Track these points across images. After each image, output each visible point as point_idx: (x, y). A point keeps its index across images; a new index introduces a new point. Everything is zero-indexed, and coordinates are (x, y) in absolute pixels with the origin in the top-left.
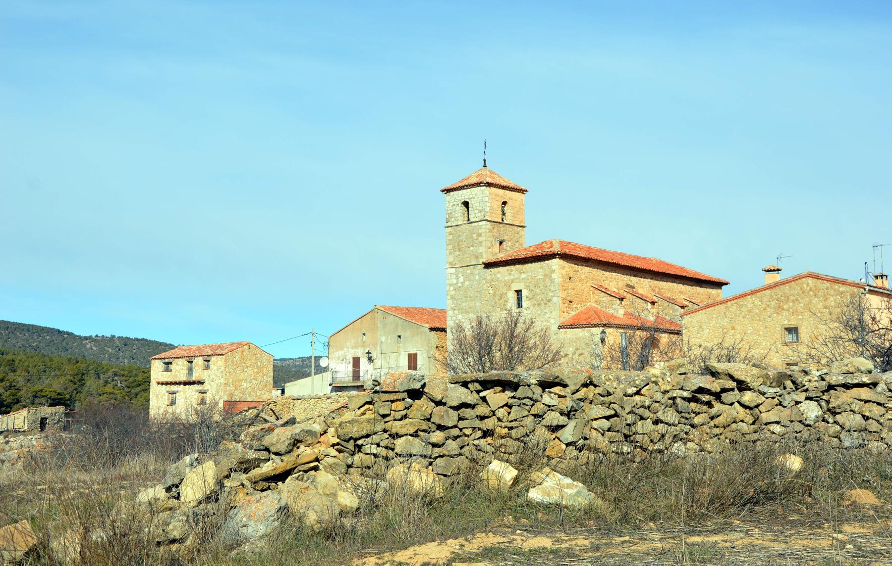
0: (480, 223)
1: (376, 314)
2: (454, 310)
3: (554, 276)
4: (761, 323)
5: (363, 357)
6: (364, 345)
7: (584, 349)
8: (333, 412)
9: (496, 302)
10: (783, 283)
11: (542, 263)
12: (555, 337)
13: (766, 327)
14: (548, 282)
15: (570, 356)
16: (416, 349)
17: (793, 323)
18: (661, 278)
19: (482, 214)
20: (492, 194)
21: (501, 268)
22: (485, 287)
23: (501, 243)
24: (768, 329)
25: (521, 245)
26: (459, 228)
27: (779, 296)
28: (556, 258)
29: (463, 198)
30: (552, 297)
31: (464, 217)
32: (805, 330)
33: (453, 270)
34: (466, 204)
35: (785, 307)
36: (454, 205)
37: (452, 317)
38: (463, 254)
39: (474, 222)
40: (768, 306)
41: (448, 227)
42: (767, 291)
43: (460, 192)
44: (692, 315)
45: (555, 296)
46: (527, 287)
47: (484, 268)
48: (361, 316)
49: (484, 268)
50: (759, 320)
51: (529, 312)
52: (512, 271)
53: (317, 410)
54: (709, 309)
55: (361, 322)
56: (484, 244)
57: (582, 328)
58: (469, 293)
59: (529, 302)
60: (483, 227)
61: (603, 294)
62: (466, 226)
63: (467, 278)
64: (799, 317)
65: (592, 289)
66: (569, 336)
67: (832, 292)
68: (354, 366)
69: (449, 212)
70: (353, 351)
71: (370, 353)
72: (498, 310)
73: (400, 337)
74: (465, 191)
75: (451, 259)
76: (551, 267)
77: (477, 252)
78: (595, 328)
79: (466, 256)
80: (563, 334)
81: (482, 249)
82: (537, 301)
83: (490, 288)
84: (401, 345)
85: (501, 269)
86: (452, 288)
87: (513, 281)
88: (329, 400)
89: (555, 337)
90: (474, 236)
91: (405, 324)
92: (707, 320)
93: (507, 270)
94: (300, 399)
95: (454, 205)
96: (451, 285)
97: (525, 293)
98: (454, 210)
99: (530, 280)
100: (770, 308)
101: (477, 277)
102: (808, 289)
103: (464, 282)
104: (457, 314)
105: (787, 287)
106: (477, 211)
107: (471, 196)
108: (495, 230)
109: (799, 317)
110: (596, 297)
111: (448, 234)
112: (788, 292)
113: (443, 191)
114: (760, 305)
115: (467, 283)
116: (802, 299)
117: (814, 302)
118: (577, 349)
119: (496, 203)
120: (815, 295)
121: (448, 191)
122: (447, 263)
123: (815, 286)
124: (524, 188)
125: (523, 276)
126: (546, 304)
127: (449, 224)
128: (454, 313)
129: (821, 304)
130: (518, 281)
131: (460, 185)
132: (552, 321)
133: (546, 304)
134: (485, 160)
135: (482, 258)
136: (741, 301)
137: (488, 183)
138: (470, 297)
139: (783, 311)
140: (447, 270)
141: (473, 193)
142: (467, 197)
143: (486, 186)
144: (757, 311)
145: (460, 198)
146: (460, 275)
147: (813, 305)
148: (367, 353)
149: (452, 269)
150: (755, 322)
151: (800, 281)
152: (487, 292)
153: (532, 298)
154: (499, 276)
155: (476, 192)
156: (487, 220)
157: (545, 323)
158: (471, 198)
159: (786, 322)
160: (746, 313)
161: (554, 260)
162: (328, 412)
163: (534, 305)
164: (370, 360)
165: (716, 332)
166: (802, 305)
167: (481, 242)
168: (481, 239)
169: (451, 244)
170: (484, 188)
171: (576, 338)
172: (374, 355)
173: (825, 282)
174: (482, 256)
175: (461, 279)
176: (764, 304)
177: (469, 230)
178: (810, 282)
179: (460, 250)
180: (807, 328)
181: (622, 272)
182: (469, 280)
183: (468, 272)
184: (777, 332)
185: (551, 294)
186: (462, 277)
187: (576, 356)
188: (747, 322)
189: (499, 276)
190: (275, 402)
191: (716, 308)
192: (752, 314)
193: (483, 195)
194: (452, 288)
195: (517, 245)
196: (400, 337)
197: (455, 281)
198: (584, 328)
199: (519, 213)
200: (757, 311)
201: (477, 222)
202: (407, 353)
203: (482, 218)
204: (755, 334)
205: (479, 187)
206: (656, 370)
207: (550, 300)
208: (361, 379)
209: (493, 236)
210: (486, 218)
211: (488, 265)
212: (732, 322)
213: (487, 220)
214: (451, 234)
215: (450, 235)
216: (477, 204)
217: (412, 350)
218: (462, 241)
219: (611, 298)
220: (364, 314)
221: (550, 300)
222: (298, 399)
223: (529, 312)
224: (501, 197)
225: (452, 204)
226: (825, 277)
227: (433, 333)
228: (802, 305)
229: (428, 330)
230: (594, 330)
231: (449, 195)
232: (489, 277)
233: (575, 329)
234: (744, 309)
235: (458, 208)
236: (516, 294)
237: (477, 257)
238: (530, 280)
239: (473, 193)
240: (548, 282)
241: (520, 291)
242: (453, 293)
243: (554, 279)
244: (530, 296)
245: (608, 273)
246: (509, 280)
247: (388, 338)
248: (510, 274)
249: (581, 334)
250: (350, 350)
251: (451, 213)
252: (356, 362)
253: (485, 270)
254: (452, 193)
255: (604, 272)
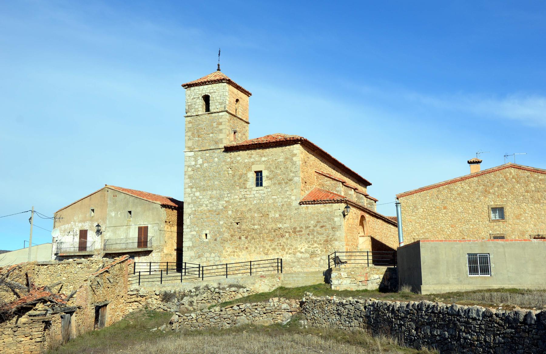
0: (221, 114)
1: (106, 193)
2: (192, 188)
4: (470, 204)
5: (91, 230)
6: (92, 219)
7: (326, 222)
8: (98, 276)
9: (235, 182)
10: (483, 173)
11: (284, 148)
13: (474, 207)
14: (289, 164)
15: (311, 228)
17: (499, 204)
19: (223, 106)
23: (235, 133)
24: (477, 209)
25: (246, 137)
26: (198, 118)
27: (486, 182)
28: (297, 144)
29: (204, 92)
31: (203, 109)
32: (510, 210)
33: (192, 154)
34: (206, 99)
35: (491, 191)
36: (195, 98)
37: (189, 194)
38: (202, 140)
39: (215, 113)
40: (476, 190)
42: (475, 178)
43: (201, 87)
44: (407, 197)
45: (296, 176)
46: (268, 168)
48: (90, 194)
50: (468, 202)
51: (269, 190)
52: (252, 154)
53: (65, 275)
54: (423, 192)
55: (90, 199)
56: (224, 131)
57: (324, 203)
58: (207, 174)
59: (270, 181)
60: (223, 117)
61: (326, 178)
62: (206, 116)
63: (206, 160)
64: (504, 199)
65: (316, 174)
66: (310, 211)
67: (533, 180)
68: (80, 237)
69: (190, 104)
70: (80, 225)
71: (100, 226)
72: (238, 188)
73: (130, 212)
74: (206, 87)
75: (190, 144)
76: (292, 151)
77: (217, 138)
78: (336, 204)
79: (205, 141)
80: (304, 209)
81: (221, 136)
82: (278, 181)
85: (241, 153)
86: (190, 169)
87: (253, 163)
88: (80, 266)
90: (215, 125)
91: (136, 201)
92: (421, 201)
93: (248, 154)
94: (46, 265)
95: (195, 98)
96: (189, 166)
97: (265, 174)
98: (194, 103)
99: (271, 162)
100: (478, 192)
101: (216, 160)
102: (511, 177)
103: (203, 163)
104: (195, 192)
105: (492, 175)
106: (217, 104)
107: (211, 91)
108: (231, 122)
109: (504, 199)
110: (320, 181)
111: (188, 122)
112: (493, 179)
113: (184, 86)
114: (468, 189)
115: (206, 165)
116: (506, 184)
117: (517, 187)
118: (318, 222)
119: (232, 98)
120: (518, 182)
123: (517, 175)
124: (250, 92)
125: (263, 159)
127: (189, 114)
128: (191, 191)
129: (523, 189)
130: (258, 163)
132: (293, 198)
134: (219, 65)
135: (222, 143)
136: (452, 186)
137: (229, 80)
138: (209, 177)
139: (490, 194)
140: (185, 153)
141: (214, 88)
142: (208, 91)
143: (227, 83)
144: (467, 194)
145: (201, 92)
147: (515, 190)
148: (97, 226)
150: (465, 203)
151: (504, 171)
152: (226, 173)
153: (273, 178)
154: (239, 158)
155: (217, 87)
156: (227, 111)
157: (286, 200)
159: (492, 203)
160: (457, 195)
161: (295, 146)
162: (94, 277)
163: (274, 184)
164: (99, 232)
165: (430, 211)
166: (506, 190)
167: (221, 130)
168: (221, 127)
170: (225, 84)
171: (317, 212)
172: (103, 228)
173: (526, 171)
175: (200, 161)
176: (472, 188)
177: (209, 120)
178: (512, 171)
179: (199, 136)
180: (511, 208)
183: (208, 155)
184: (485, 211)
185: (292, 174)
186: (201, 160)
187: (318, 228)
188: (457, 203)
189: (239, 158)
190: (20, 268)
191: (429, 191)
192: (462, 197)
193: (224, 90)
194: (190, 169)
196: (130, 212)
197: (193, 163)
199: (245, 111)
200: (467, 194)
201: (218, 112)
202: (137, 226)
203: (223, 109)
204: (465, 212)
206: (188, 255)
207: (290, 180)
208: (88, 249)
209: (231, 126)
210: (226, 109)
211: (228, 149)
212: (443, 203)
213: (227, 111)
214: (190, 122)
215: (189, 123)
216: (218, 98)
217: (143, 225)
220: (70, 204)
221: (290, 180)
222: (43, 265)
223: (269, 190)
225: (192, 97)
226: (526, 167)
228: (506, 190)
229: (160, 206)
230: (336, 205)
234: (454, 192)
235: (198, 101)
236: (255, 174)
237: (216, 143)
238: (271, 162)
239: (214, 88)
240: (289, 164)
241: (261, 172)
242: (192, 173)
243: (296, 162)
244: (271, 176)
245: (322, 164)
246: (249, 162)
247: (118, 213)
248: (250, 157)
249: (322, 209)
250: (77, 223)
252: (83, 234)
253: (225, 153)
254: (192, 88)
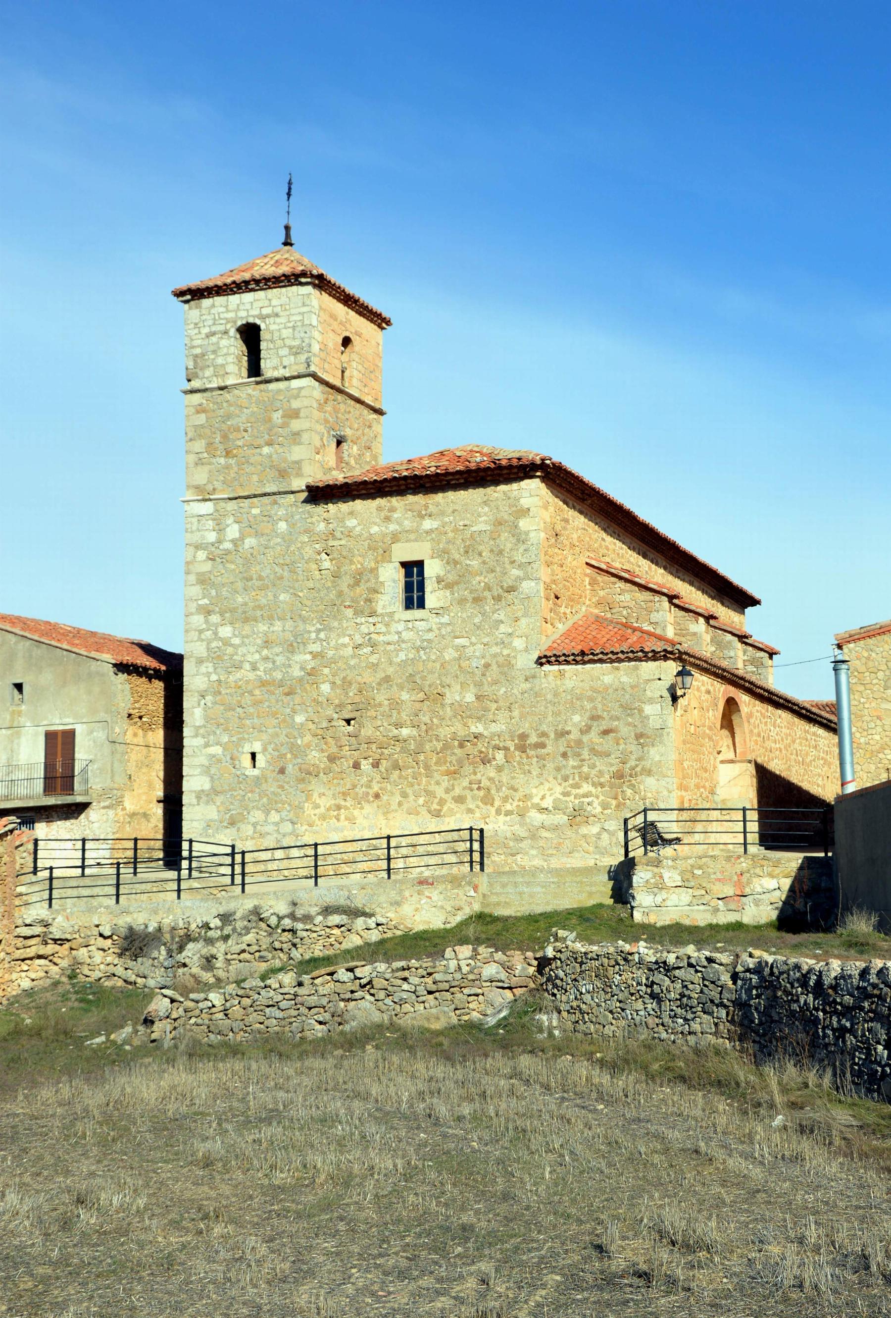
0: (295, 383)
2: (209, 613)
3: (523, 524)
7: (618, 719)
9: (340, 594)
11: (490, 490)
12: (526, 686)
14: (506, 540)
15: (572, 736)
16: (71, 721)
18: (677, 571)
19: (303, 358)
20: (325, 310)
21: (358, 502)
22: (308, 552)
23: (339, 443)
25: (375, 457)
29: (243, 314)
30: (520, 579)
31: (240, 369)
36: (213, 334)
37: (201, 632)
38: (239, 464)
39: (277, 380)
41: (192, 391)
43: (234, 299)
45: (527, 578)
46: (442, 554)
47: (306, 501)
49: (306, 501)
51: (445, 619)
52: (392, 510)
56: (305, 437)
57: (612, 661)
58: (254, 570)
59: (448, 593)
60: (303, 393)
61: (621, 584)
62: (250, 390)
63: (250, 527)
65: (589, 571)
66: (569, 684)
69: (198, 351)
72: (349, 613)
73: (19, 687)
74: (248, 297)
75: (201, 477)
76: (517, 500)
77: (285, 460)
78: (651, 664)
79: (249, 469)
80: (551, 678)
81: (297, 453)
83: (324, 556)
84: (23, 707)
86: (201, 555)
87: (395, 538)
89: (526, 686)
90: (277, 417)
93: (379, 509)
95: (213, 334)
96: (198, 547)
97: (432, 570)
98: (212, 348)
101: (282, 526)
103: (242, 539)
104: (216, 626)
106: (284, 352)
107: (265, 311)
108: (329, 408)
110: (602, 593)
113: (179, 294)
115: (250, 542)
118: (594, 718)
119: (331, 334)
121: (196, 294)
122: (188, 487)
124: (385, 314)
125: (428, 524)
126: (498, 599)
127: (196, 384)
128: (207, 622)
130: (412, 536)
131: (238, 278)
132: (519, 643)
133: (498, 599)
134: (287, 228)
135: (299, 475)
138: (260, 578)
140: (186, 507)
141: (274, 302)
145: (231, 315)
146: (230, 520)
149: (202, 504)
154: (351, 523)
155: (284, 299)
156: (314, 376)
157: (495, 649)
158: (268, 316)
161: (527, 484)
167: (297, 434)
168: (296, 425)
169: (200, 436)
170: (309, 289)
174: (300, 469)
175: (233, 531)
177: (258, 402)
179: (228, 454)
181: (628, 540)
182: (257, 534)
183: (255, 511)
185: (515, 572)
186: (236, 527)
187: (593, 736)
189: (351, 523)
193: (305, 309)
194: (201, 555)
195: (368, 456)
196: (19, 687)
197: (212, 537)
198: (620, 661)
199: (372, 376)
201: (287, 379)
202: (42, 731)
203: (302, 369)
205: (294, 288)
207: (511, 590)
209: (326, 421)
210: (313, 368)
213: (314, 376)
215: (198, 412)
216: (286, 333)
218: (237, 430)
219: (644, 596)
221: (511, 590)
224: (341, 323)
225: (206, 330)
227: (123, 677)
229: (111, 669)
230: (649, 668)
231: (199, 307)
232: (322, 526)
233: (588, 666)
237: (283, 474)
239: (274, 302)
240: (506, 540)
241: (420, 564)
242: (207, 567)
243: (527, 533)
244: (451, 578)
246: (384, 535)
248: (388, 519)
249: (607, 679)
251: (203, 355)
253: (309, 507)
254: (206, 302)
255: (604, 535)
